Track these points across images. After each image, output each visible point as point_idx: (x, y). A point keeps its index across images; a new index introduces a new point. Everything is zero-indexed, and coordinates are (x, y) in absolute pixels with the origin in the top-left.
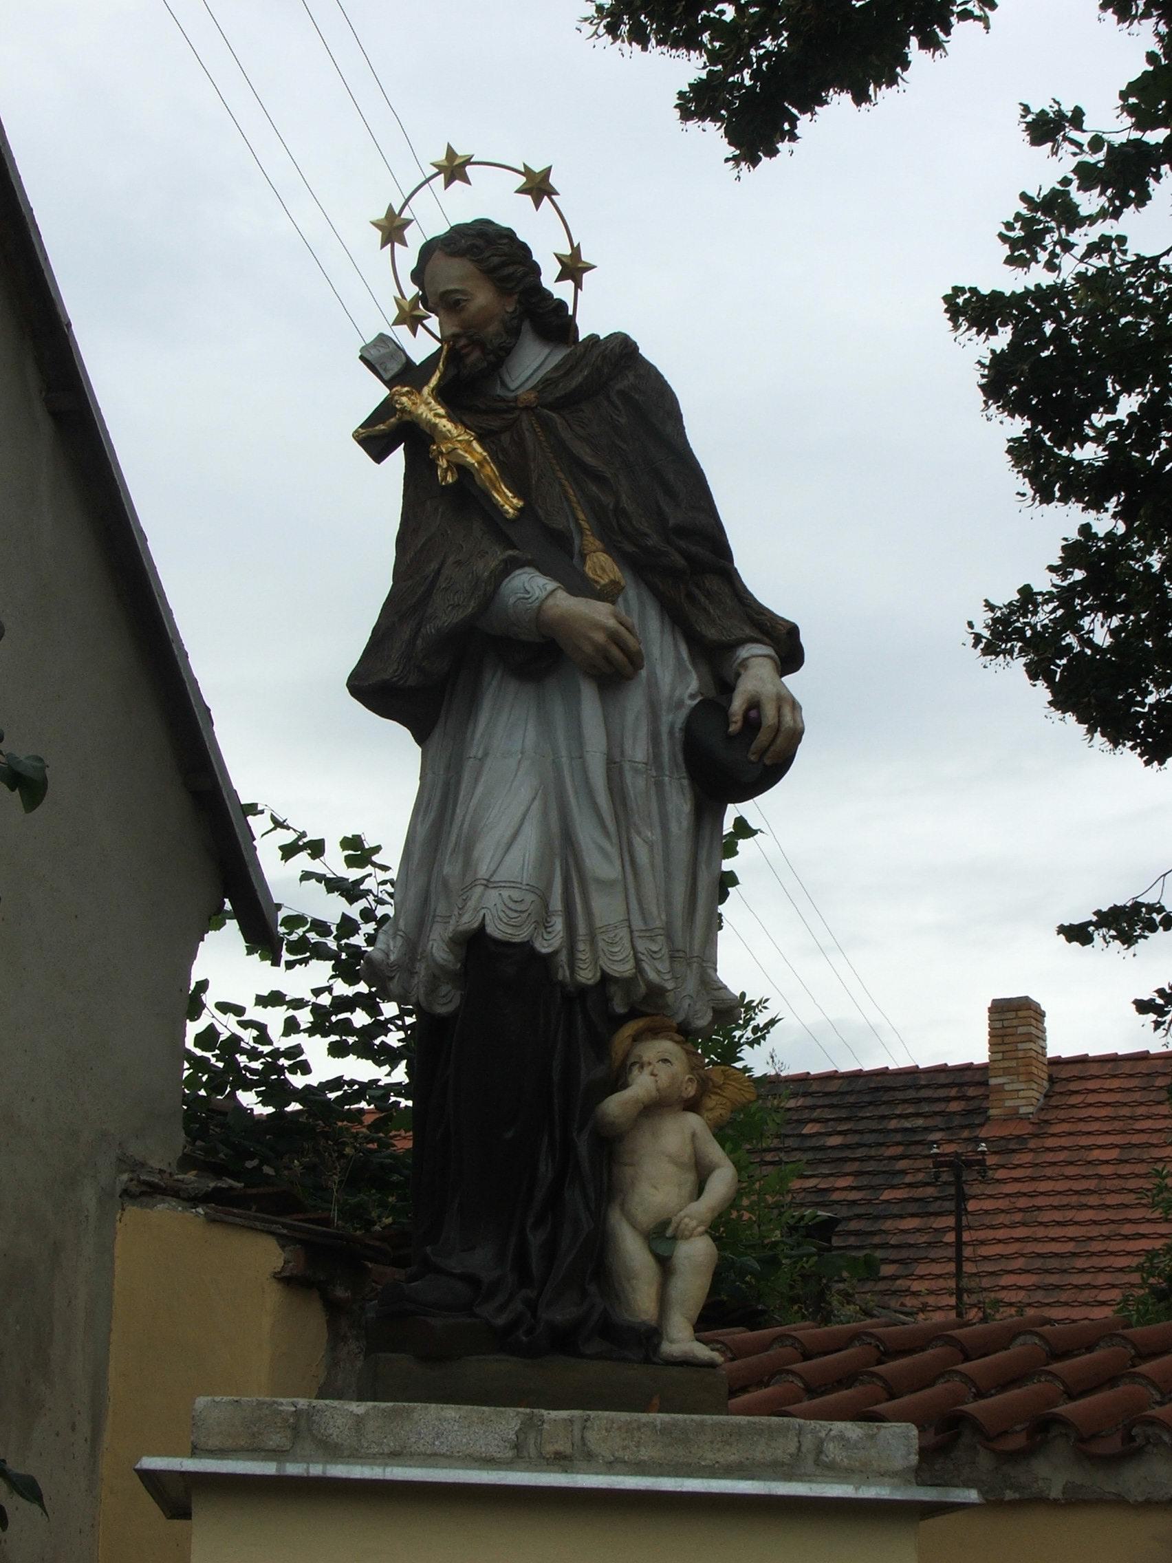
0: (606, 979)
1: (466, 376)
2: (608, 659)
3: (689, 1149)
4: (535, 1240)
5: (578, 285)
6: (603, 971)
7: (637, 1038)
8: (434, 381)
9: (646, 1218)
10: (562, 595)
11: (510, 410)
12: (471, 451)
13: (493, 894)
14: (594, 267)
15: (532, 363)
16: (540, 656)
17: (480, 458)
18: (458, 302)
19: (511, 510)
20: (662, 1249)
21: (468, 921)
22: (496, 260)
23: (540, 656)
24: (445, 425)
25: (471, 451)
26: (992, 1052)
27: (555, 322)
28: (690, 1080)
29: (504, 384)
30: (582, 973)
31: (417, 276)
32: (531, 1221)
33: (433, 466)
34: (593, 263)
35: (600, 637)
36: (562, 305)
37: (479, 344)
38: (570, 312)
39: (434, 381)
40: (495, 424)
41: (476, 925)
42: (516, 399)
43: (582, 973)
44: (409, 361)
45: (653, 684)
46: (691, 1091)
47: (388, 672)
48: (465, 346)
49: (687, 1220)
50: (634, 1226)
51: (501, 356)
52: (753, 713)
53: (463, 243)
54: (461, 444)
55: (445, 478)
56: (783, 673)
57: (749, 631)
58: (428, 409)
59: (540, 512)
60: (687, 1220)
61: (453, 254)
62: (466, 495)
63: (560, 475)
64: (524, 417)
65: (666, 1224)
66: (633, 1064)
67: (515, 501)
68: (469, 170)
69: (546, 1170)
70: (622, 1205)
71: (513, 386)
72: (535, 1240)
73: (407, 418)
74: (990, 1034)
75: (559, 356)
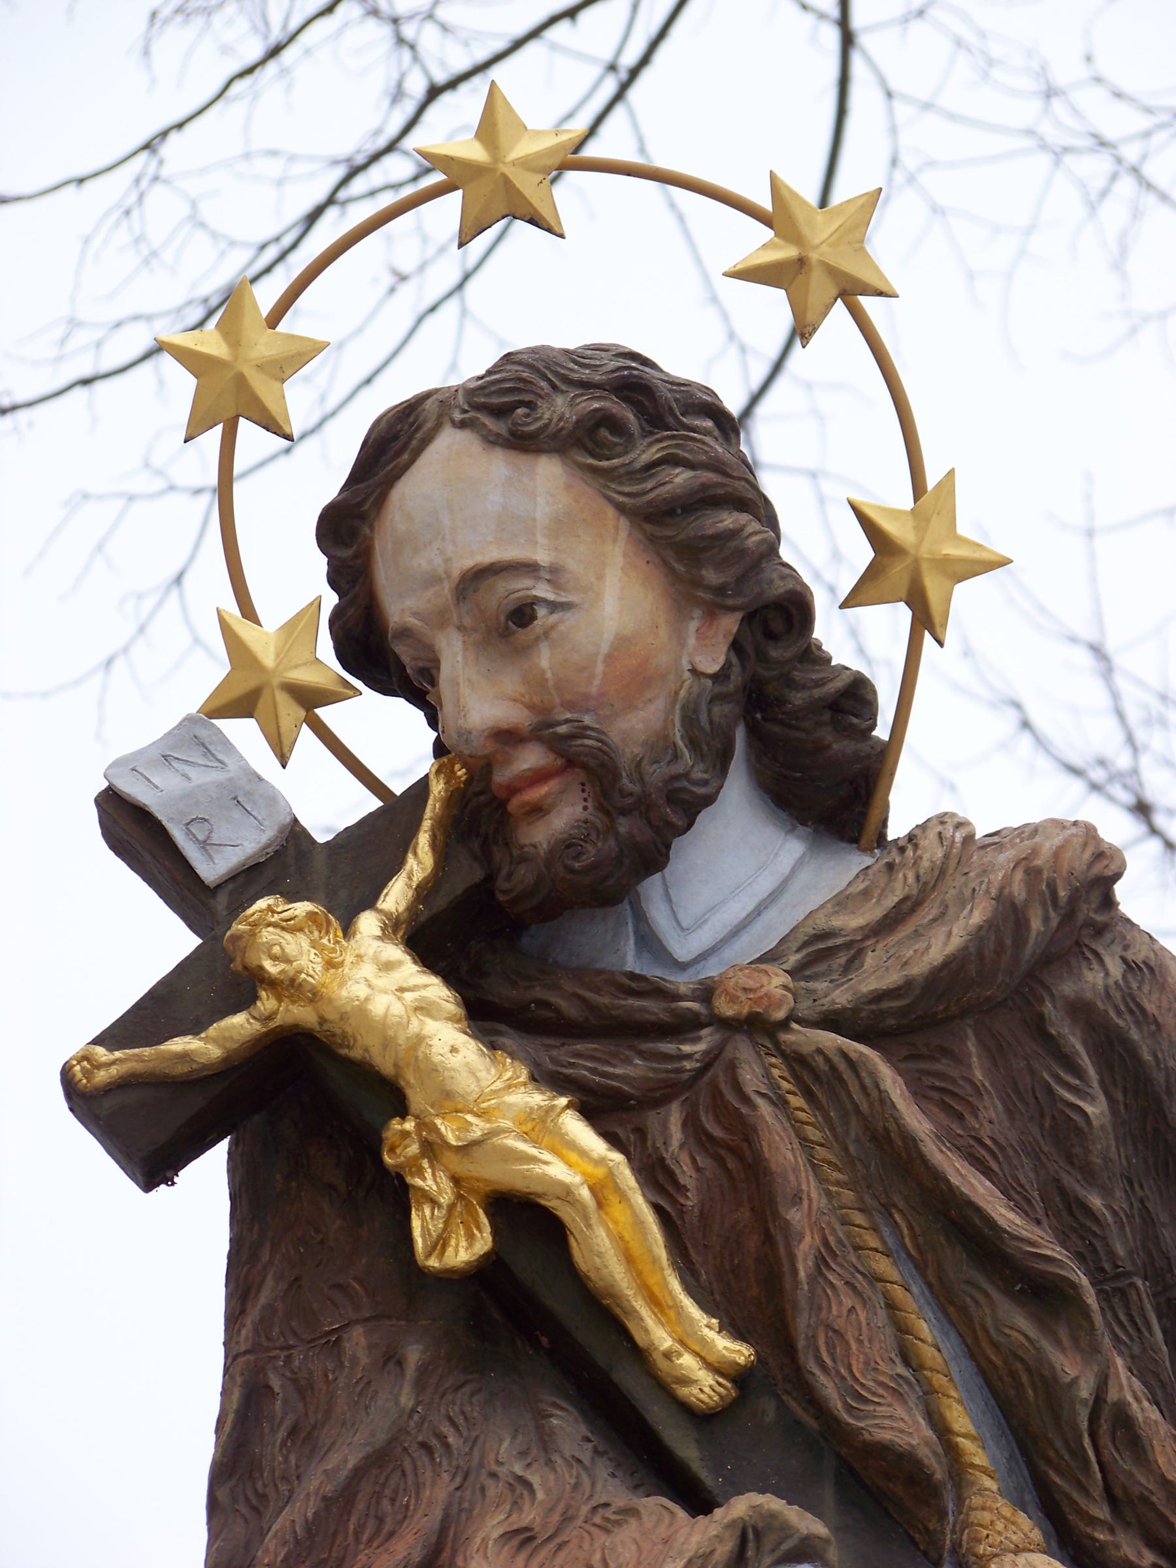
5: (926, 621)
8: (396, 896)
11: (686, 1026)
12: (564, 1146)
15: (737, 890)
17: (600, 1172)
18: (523, 614)
19: (706, 1379)
22: (681, 478)
25: (564, 1146)
29: (649, 941)
33: (397, 1196)
36: (856, 695)
38: (882, 732)
39: (396, 896)
40: (629, 1070)
42: (706, 992)
48: (539, 777)
51: (647, 826)
53: (561, 409)
55: (440, 1244)
58: (377, 983)
59: (828, 1388)
61: (523, 443)
64: (743, 1051)
68: (572, 194)
71: (683, 948)
75: (844, 869)
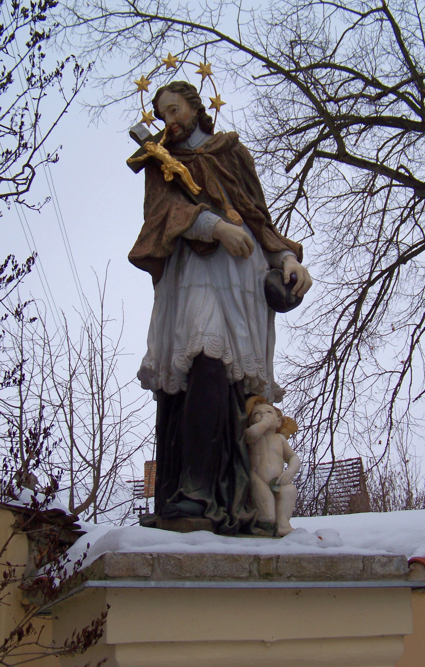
0: (246, 377)
1: (174, 141)
2: (241, 249)
3: (282, 448)
4: (224, 485)
5: (218, 110)
6: (245, 373)
7: (255, 403)
8: (162, 141)
9: (269, 477)
10: (223, 222)
11: (193, 154)
12: (181, 167)
13: (206, 338)
14: (225, 104)
15: (198, 140)
16: (209, 248)
18: (174, 110)
20: (276, 489)
21: (196, 349)
23: (209, 248)
24: (168, 157)
25: (181, 167)
26: (145, 477)
27: (207, 125)
28: (279, 420)
30: (236, 374)
31: (155, 102)
32: (220, 478)
33: (163, 173)
34: (225, 102)
35: (240, 239)
36: (210, 119)
37: (181, 126)
38: (213, 122)
39: (162, 141)
40: (187, 159)
41: (200, 351)
43: (236, 374)
44: (151, 135)
45: (253, 264)
46: (279, 425)
47: (148, 249)
48: (177, 128)
49: (285, 477)
50: (263, 480)
51: (188, 133)
52: (293, 276)
54: (173, 164)
55: (168, 178)
56: (301, 262)
57: (286, 247)
58: (160, 150)
60: (285, 477)
61: (174, 92)
62: (177, 185)
63: (215, 179)
65: (276, 478)
66: (256, 413)
67: (198, 188)
69: (226, 456)
70: (257, 472)
71: (193, 146)
72: (224, 485)
73: (151, 154)
74: (145, 472)
